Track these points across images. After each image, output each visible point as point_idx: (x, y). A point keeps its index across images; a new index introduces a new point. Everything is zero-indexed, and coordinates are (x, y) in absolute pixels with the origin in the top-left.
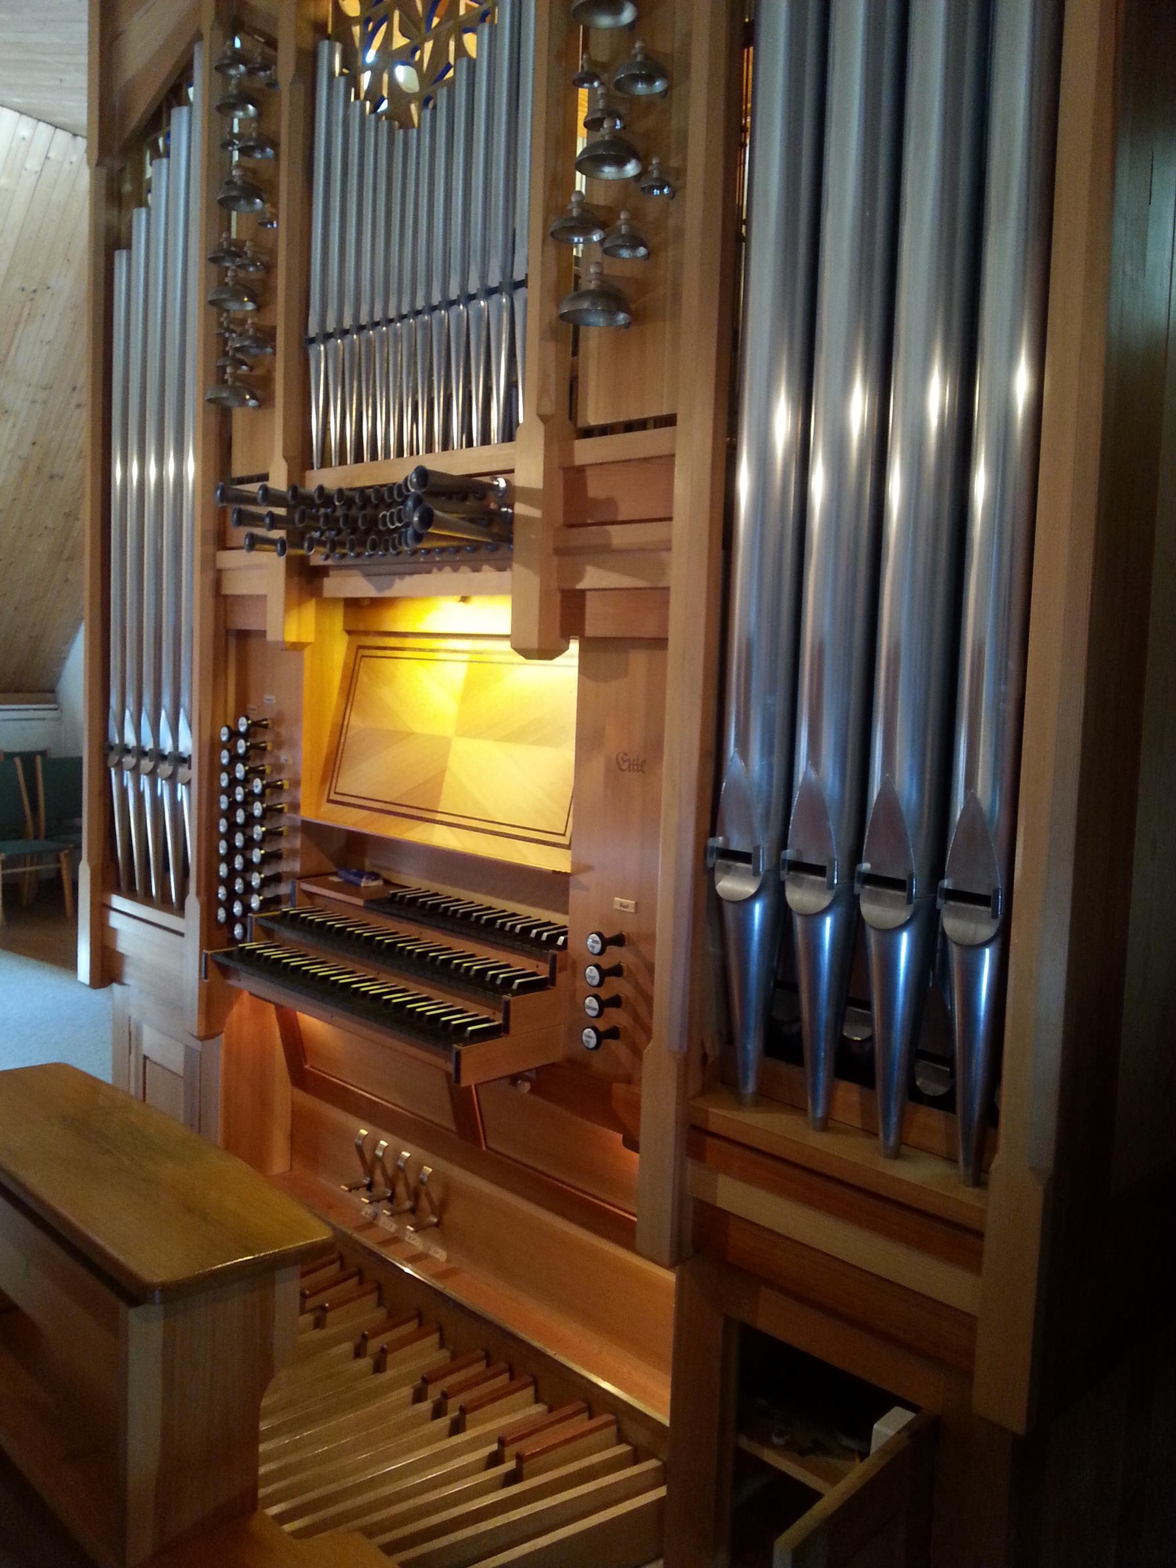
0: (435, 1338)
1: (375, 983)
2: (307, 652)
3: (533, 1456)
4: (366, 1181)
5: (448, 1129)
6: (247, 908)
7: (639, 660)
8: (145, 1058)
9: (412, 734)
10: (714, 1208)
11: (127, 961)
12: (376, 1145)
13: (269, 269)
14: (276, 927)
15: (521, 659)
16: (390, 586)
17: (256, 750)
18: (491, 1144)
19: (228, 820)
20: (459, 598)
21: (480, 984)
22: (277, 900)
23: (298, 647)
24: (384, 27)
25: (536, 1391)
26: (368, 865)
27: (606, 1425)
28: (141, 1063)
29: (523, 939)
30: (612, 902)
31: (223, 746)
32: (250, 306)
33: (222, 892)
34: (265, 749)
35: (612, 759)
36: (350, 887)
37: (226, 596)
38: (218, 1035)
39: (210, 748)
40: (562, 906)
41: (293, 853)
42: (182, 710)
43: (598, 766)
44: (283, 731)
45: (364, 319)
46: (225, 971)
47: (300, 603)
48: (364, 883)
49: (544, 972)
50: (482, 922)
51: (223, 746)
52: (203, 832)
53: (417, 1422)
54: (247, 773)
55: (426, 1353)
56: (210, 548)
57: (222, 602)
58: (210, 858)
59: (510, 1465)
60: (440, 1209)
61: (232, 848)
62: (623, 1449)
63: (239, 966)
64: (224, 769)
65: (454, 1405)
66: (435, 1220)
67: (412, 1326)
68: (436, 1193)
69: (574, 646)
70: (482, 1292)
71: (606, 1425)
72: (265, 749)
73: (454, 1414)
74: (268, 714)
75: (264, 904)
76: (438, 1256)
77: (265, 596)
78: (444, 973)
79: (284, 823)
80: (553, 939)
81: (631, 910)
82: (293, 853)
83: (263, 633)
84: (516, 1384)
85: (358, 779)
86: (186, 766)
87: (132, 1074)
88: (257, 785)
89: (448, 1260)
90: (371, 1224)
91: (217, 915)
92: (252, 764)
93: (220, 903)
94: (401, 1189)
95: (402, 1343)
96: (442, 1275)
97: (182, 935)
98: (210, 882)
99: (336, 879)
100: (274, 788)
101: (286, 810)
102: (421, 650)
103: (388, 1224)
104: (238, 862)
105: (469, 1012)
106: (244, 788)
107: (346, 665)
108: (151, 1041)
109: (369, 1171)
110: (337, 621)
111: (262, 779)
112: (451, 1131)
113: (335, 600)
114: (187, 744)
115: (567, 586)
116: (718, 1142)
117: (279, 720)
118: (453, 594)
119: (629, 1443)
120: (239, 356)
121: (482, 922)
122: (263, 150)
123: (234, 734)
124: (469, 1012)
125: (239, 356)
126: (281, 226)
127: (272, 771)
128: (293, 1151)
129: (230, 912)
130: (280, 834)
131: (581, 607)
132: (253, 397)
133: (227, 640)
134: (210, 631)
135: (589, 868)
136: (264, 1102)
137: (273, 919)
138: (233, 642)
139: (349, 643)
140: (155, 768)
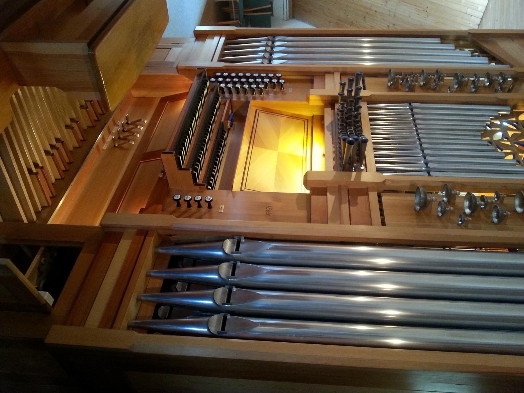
2: (306, 103)
4: (129, 122)
6: (220, 82)
7: (303, 213)
8: (171, 49)
11: (203, 43)
12: (141, 126)
13: (434, 90)
14: (214, 92)
15: (304, 174)
16: (328, 130)
17: (274, 86)
21: (195, 161)
22: (223, 92)
23: (308, 100)
24: (515, 128)
25: (59, 179)
26: (235, 123)
30: (223, 204)
31: (275, 75)
32: (422, 84)
35: (270, 205)
36: (228, 117)
37: (325, 75)
39: (274, 72)
41: (239, 98)
43: (268, 200)
44: (280, 95)
45: (417, 122)
46: (199, 75)
47: (323, 100)
48: (229, 122)
51: (275, 75)
53: (49, 139)
54: (266, 82)
55: (72, 142)
56: (341, 70)
57: (323, 74)
58: (237, 70)
60: (120, 147)
67: (81, 138)
68: (125, 146)
69: (308, 192)
70: (93, 160)
71: (48, 203)
72: (274, 88)
73: (52, 152)
75: (222, 89)
79: (249, 95)
80: (210, 185)
81: (220, 211)
82: (239, 98)
84: (62, 172)
85: (264, 120)
88: (261, 86)
89: (103, 150)
90: (115, 124)
92: (269, 84)
93: (222, 73)
94: (127, 134)
96: (98, 148)
97: (212, 61)
98: (229, 70)
99: (230, 112)
100: (261, 91)
103: (115, 130)
104: (236, 80)
105: (186, 157)
107: (302, 115)
108: (176, 51)
109: (133, 123)
110: (317, 113)
113: (323, 112)
114: (275, 62)
120: (405, 80)
122: (474, 88)
123: (279, 78)
124: (186, 157)
125: (405, 80)
126: (448, 94)
128: (139, 98)
130: (245, 94)
131: (321, 194)
132: (391, 85)
134: (313, 70)
135: (234, 197)
136: (156, 88)
138: (309, 78)
140: (268, 52)
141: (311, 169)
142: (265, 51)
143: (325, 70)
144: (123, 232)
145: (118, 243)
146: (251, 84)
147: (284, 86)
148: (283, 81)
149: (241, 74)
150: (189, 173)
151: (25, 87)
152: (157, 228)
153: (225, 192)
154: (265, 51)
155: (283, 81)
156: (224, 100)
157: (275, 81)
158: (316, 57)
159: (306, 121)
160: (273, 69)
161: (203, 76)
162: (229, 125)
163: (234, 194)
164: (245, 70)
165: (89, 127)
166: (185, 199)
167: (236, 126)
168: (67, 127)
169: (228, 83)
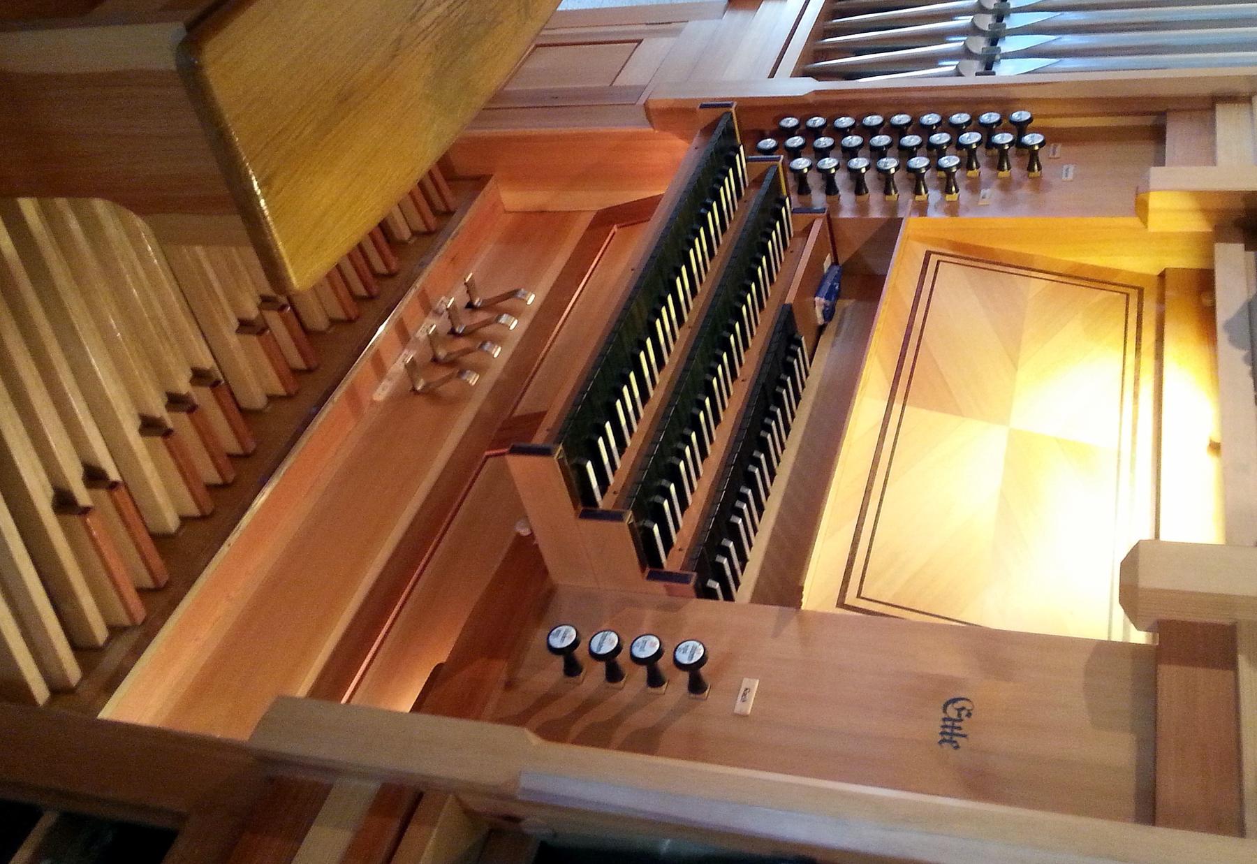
0: (281, 391)
1: (672, 329)
2: (1134, 221)
3: (87, 528)
4: (477, 302)
5: (515, 408)
6: (795, 153)
7: (1116, 751)
8: (640, 42)
9: (1016, 368)
12: (513, 313)
16: (1233, 341)
17: (1000, 158)
18: (490, 460)
19: (908, 125)
20: (1217, 440)
21: (660, 471)
23: (1141, 209)
26: (846, 304)
27: (130, 615)
28: (632, 38)
29: (722, 530)
30: (752, 674)
31: (1005, 116)
33: (901, 119)
37: (1213, 109)
39: (1004, 103)
40: (759, 597)
41: (863, 208)
42: (1054, 60)
43: (951, 664)
44: (1024, 192)
47: (1204, 211)
49: (670, 563)
50: (751, 468)
51: (1005, 116)
53: (161, 374)
54: (968, 146)
55: (256, 378)
57: (1204, 105)
58: (859, 105)
59: (83, 496)
60: (430, 394)
61: (900, 131)
62: (101, 634)
63: (711, 147)
64: (975, 117)
65: (177, 421)
66: (419, 388)
68: (451, 389)
69: (1140, 637)
71: (130, 615)
72: (1001, 168)
73: (169, 420)
74: (1048, 170)
75: (800, 176)
76: (379, 390)
77: (1214, 163)
78: (680, 420)
79: (903, 196)
81: (739, 707)
82: (863, 208)
83: (1160, 162)
85: (956, 291)
86: (982, 70)
88: (950, 161)
89: (373, 403)
90: (427, 307)
93: (803, 121)
94: (462, 343)
96: (353, 395)
97: (772, 75)
98: (830, 106)
100: (947, 182)
101: (918, 198)
102: (1137, 380)
103: (432, 325)
104: (854, 140)
106: (949, 143)
107: (1116, 272)
108: (655, 49)
109: (489, 306)
110: (1181, 260)
111: (958, 166)
112: (513, 412)
113: (1210, 256)
114: (1007, 70)
115: (1243, 643)
119: (109, 640)
121: (751, 468)
123: (1021, 129)
128: (526, 214)
129: (791, 132)
130: (887, 192)
131: (1208, 662)
133: (1151, 113)
134: (1163, 91)
138: (1149, 121)
141: (1157, 536)
144: (330, 787)
145: (300, 840)
146: (940, 151)
147: (1041, 156)
150: (619, 535)
151: (61, 202)
153: (772, 612)
154: (974, 30)
156: (804, 219)
157: (1003, 138)
158: (1174, 41)
159: (1134, 295)
160: (999, 94)
161: (718, 132)
162: (819, 315)
163: (804, 618)
166: (594, 649)
167: (848, 315)
168: (245, 326)
169: (852, 152)
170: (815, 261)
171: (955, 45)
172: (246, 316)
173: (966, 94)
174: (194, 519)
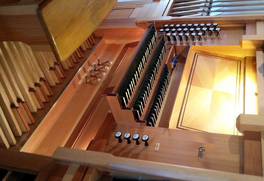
2: (239, 46)
3: (18, 111)
4: (100, 64)
5: (108, 86)
6: (167, 32)
7: (236, 158)
9: (214, 77)
10: (65, 174)
12: (108, 66)
14: (161, 40)
15: (237, 117)
16: (260, 72)
17: (211, 33)
19: (191, 26)
20: (257, 93)
21: (139, 99)
22: (169, 40)
23: (241, 44)
26: (178, 64)
29: (152, 112)
31: (212, 24)
34: (211, 35)
37: (256, 23)
38: (137, 26)
39: (212, 22)
40: (160, 126)
41: (182, 44)
43: (200, 140)
44: (216, 40)
46: (149, 27)
47: (254, 44)
48: (173, 63)
49: (141, 118)
50: (158, 98)
51: (212, 24)
52: (189, 20)
53: (33, 79)
54: (204, 31)
55: (53, 79)
58: (181, 22)
59: (17, 104)
60: (90, 83)
62: (20, 133)
64: (205, 24)
65: (36, 89)
66: (88, 82)
68: (94, 82)
69: (240, 134)
70: (69, 93)
72: (211, 35)
73: (35, 88)
76: (79, 82)
77: (256, 34)
78: (143, 89)
79: (190, 41)
80: (151, 121)
81: (156, 149)
82: (182, 44)
83: (245, 34)
84: (42, 103)
85: (202, 63)
86: (207, 14)
87: (132, 6)
88: (200, 34)
89: (78, 85)
90: (89, 64)
91: (178, 24)
92: (207, 32)
93: (169, 25)
94: (97, 72)
95: (57, 74)
96: (74, 84)
97: (162, 16)
98: (175, 22)
103: (90, 68)
104: (180, 29)
105: (130, 96)
106: (200, 30)
107: (235, 57)
108: (138, 10)
109: (102, 64)
110: (249, 55)
111: (202, 35)
113: (255, 54)
114: (212, 15)
116: (82, 177)
117: (219, 39)
118: (258, 91)
119: (22, 135)
123: (215, 27)
124: (130, 96)
127: (205, 37)
129: (166, 28)
130: (187, 40)
131: (255, 139)
134: (245, 19)
135: (169, 135)
136: (122, 38)
137: (163, 38)
138: (242, 25)
139: (242, 58)
140: (207, 7)
141: (244, 113)
142: (205, 6)
143: (257, 18)
144: (69, 166)
146: (198, 32)
147: (220, 33)
148: (219, 29)
149: (202, 25)
150: (130, 113)
151: (12, 42)
152: (95, 167)
154: (205, 6)
155: (219, 29)
156: (169, 46)
157: (211, 29)
159: (239, 62)
162: (173, 66)
163: (170, 131)
164: (187, 21)
165: (70, 68)
167: (178, 66)
168: (51, 69)
170: (172, 55)
171: (201, 9)
172: (51, 66)
173: (204, 20)
174: (40, 109)
